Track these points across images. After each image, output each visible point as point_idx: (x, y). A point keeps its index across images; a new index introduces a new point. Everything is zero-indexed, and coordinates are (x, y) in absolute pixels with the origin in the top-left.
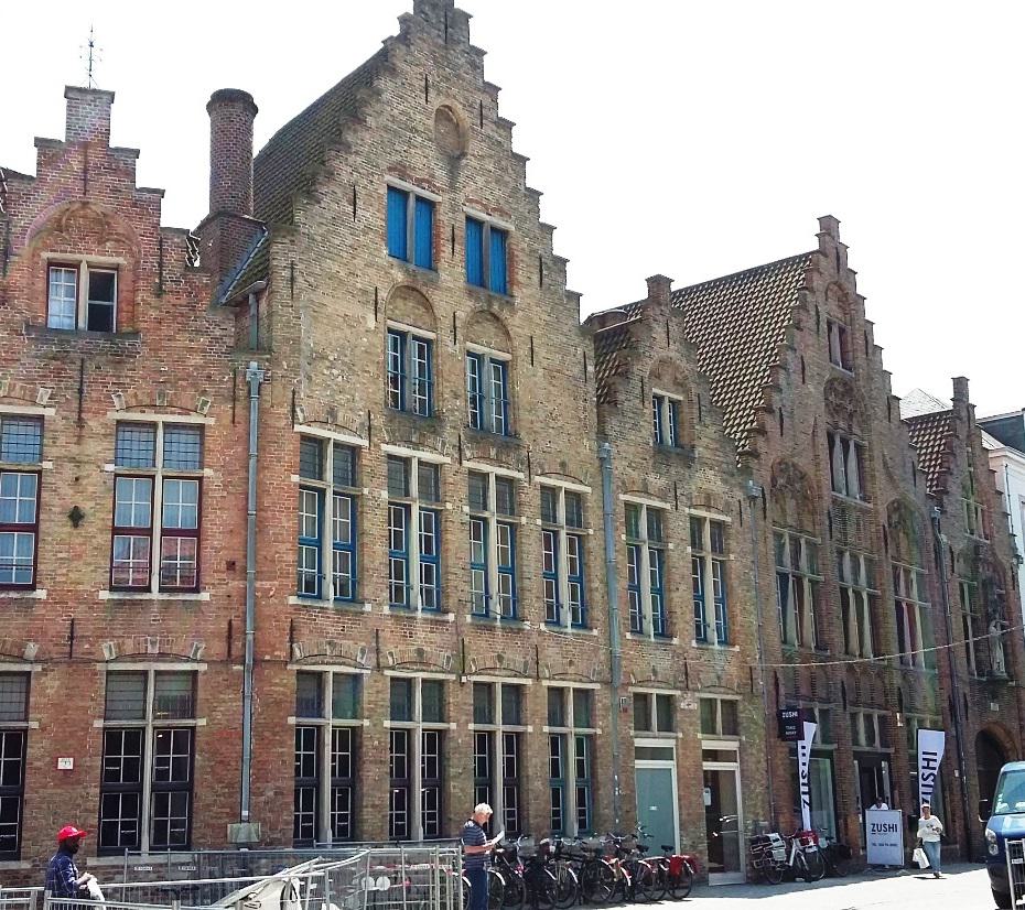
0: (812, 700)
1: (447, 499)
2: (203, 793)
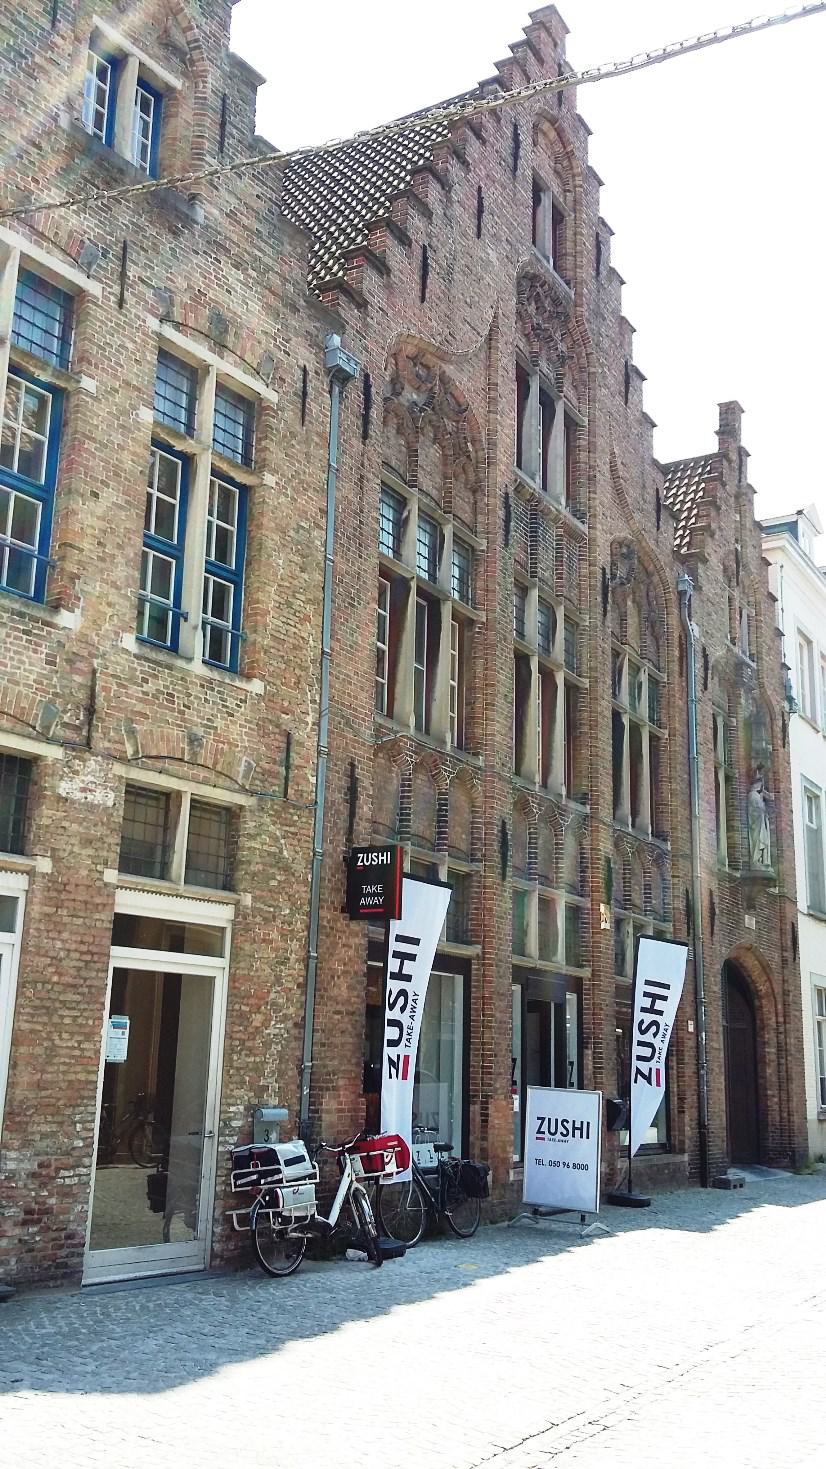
0: (435, 848)
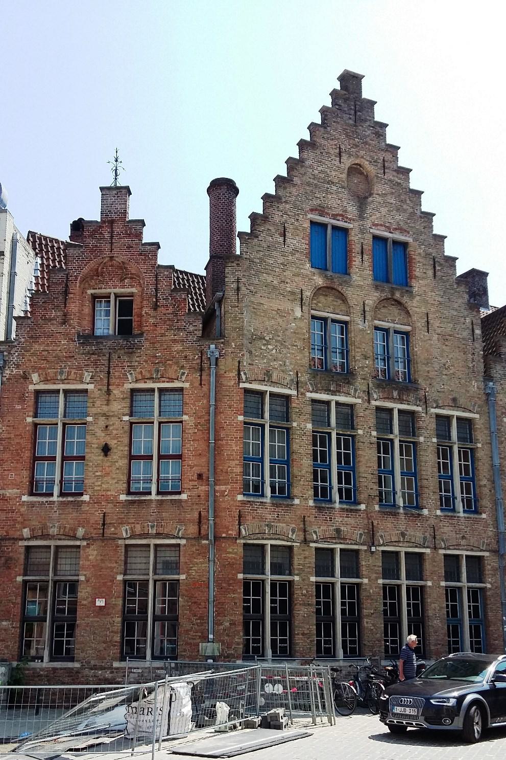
1: (359, 427)
2: (184, 623)
